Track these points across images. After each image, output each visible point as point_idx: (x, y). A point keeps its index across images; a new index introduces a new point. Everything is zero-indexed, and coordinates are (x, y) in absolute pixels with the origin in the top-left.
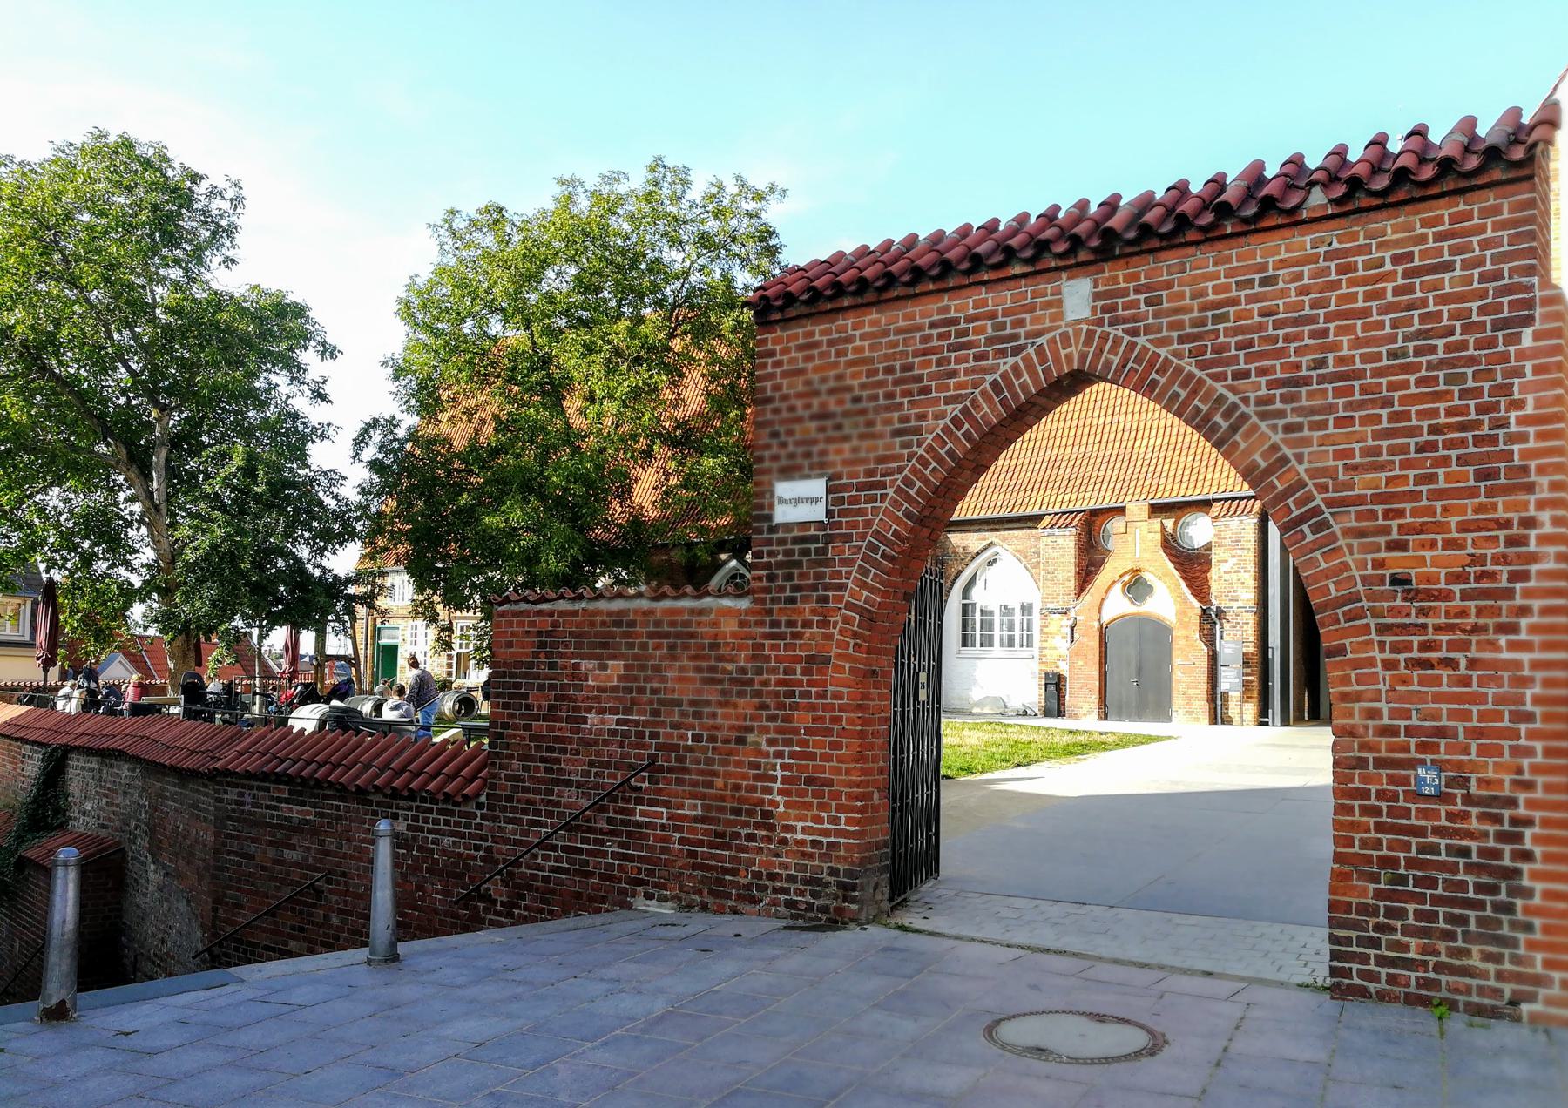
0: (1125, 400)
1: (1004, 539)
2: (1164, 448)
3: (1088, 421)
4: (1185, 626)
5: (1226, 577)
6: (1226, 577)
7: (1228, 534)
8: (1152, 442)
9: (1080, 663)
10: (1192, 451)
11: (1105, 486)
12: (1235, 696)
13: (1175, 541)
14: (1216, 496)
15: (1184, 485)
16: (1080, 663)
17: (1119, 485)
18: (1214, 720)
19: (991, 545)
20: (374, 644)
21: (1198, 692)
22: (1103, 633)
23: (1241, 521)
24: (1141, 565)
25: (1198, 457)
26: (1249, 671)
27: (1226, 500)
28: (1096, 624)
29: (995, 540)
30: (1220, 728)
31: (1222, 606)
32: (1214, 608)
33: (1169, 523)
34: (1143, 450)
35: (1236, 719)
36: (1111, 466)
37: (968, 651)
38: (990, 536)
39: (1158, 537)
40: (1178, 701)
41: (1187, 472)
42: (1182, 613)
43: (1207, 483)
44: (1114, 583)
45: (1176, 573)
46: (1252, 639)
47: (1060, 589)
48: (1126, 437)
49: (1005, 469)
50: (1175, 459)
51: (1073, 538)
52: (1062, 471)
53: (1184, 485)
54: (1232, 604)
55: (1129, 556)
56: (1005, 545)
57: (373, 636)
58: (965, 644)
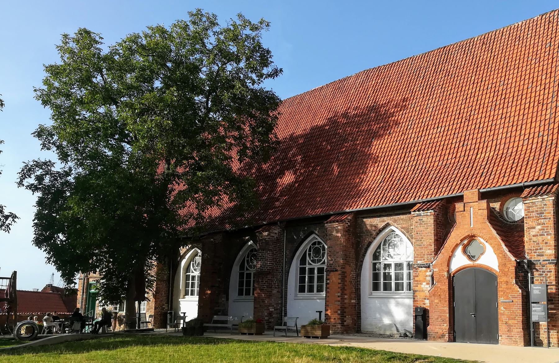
0: (472, 132)
1: (395, 221)
2: (495, 157)
3: (449, 146)
4: (505, 274)
5: (535, 239)
6: (535, 239)
7: (535, 209)
8: (487, 155)
9: (436, 301)
10: (512, 158)
11: (455, 183)
12: (543, 324)
13: (502, 216)
14: (526, 184)
15: (506, 179)
16: (436, 301)
17: (464, 182)
18: (527, 343)
19: (388, 225)
20: (87, 292)
21: (516, 322)
22: (451, 279)
23: (543, 199)
24: (475, 232)
25: (516, 161)
26: (552, 306)
27: (533, 186)
28: (446, 274)
29: (390, 222)
30: (532, 349)
31: (533, 260)
32: (526, 261)
33: (496, 205)
34: (481, 160)
35: (545, 342)
36: (460, 171)
37: (376, 293)
38: (387, 220)
39: (485, 212)
40: (502, 328)
41: (508, 170)
42: (502, 265)
43: (521, 176)
44: (457, 246)
45: (498, 237)
46: (554, 283)
47: (426, 252)
48: (471, 153)
49: (398, 178)
50: (501, 163)
51: (432, 217)
52: (430, 177)
53: (506, 179)
54: (539, 258)
55: (466, 226)
56: (395, 225)
57: (87, 288)
58: (302, 290)
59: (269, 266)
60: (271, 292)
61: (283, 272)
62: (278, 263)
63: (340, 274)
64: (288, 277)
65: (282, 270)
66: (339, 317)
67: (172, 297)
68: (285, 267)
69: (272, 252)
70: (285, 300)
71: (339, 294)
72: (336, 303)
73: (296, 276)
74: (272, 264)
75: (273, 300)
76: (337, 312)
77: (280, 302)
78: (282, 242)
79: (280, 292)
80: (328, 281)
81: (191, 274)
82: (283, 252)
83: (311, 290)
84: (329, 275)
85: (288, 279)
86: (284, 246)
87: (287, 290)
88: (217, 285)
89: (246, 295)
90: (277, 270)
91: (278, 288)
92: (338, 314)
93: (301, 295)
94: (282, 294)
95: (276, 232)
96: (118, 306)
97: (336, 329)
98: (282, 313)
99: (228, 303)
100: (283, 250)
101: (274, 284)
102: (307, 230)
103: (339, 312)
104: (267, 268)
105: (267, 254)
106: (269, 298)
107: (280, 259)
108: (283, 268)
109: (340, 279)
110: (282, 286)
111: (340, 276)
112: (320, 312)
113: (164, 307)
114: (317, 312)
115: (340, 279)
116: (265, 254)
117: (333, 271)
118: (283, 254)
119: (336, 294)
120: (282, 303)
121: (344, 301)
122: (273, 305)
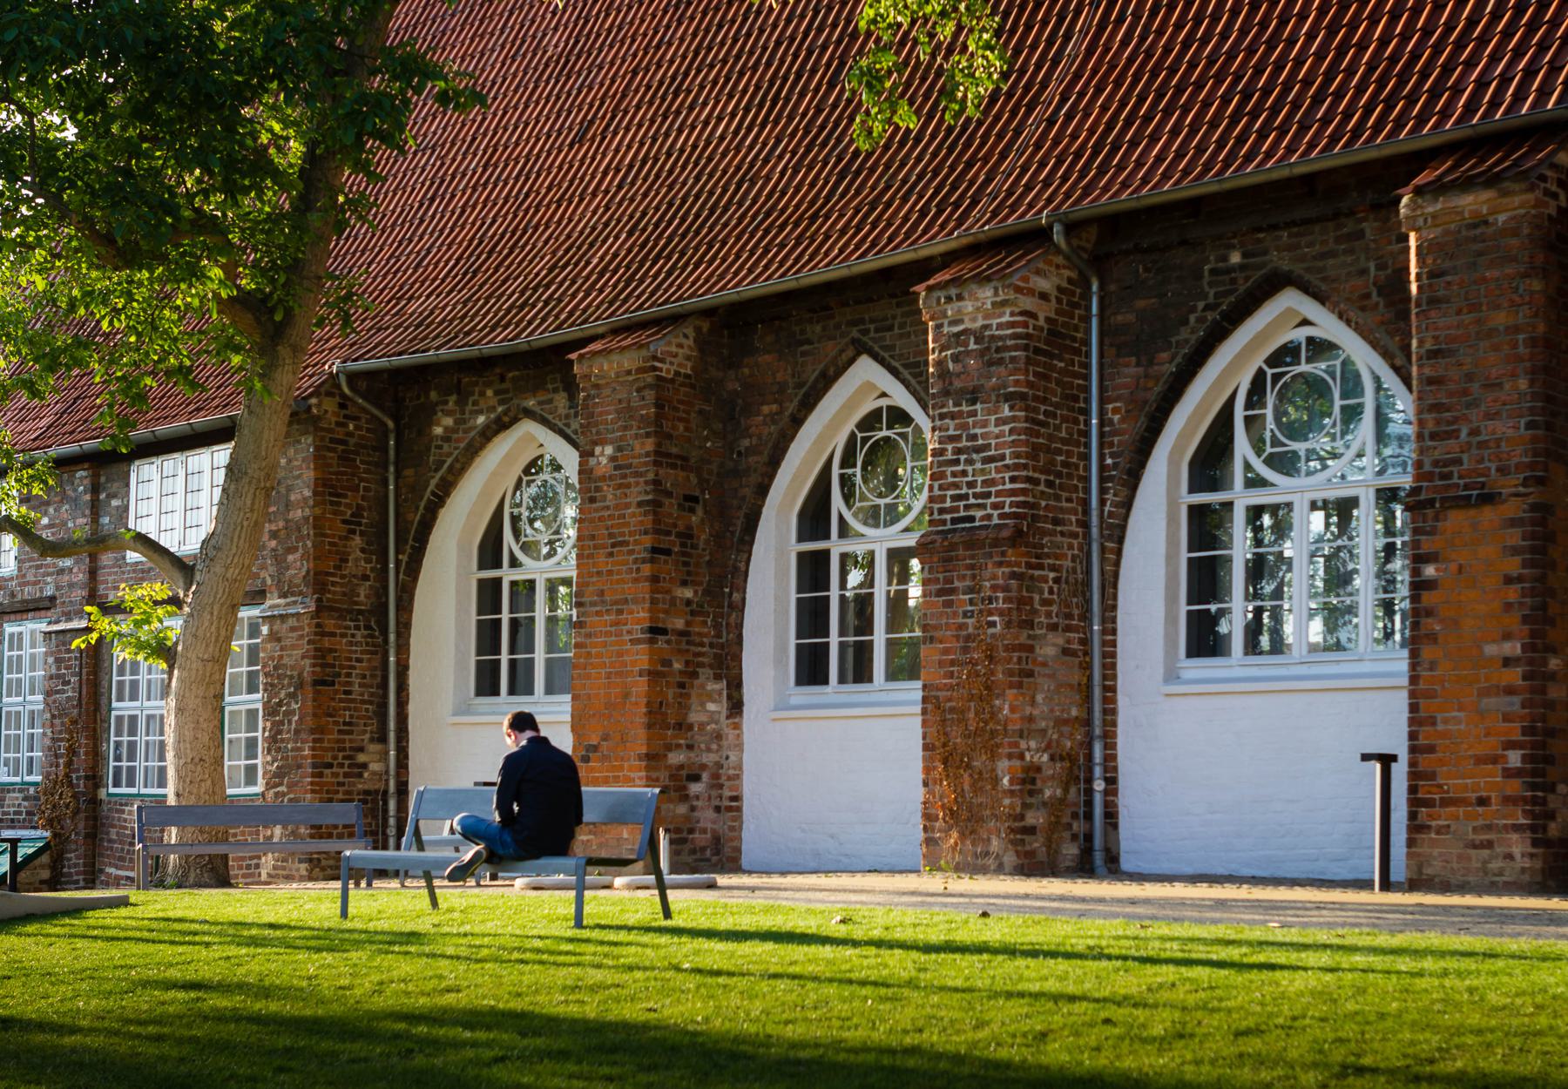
59: (1013, 493)
60: (1031, 649)
61: (1087, 535)
62: (1059, 475)
63: (1513, 522)
64: (1117, 564)
65: (1085, 525)
66: (1515, 787)
67: (402, 703)
68: (1102, 502)
69: (1027, 409)
70: (1105, 700)
71: (1513, 648)
72: (1491, 702)
73: (1171, 557)
74: (1028, 480)
75: (1039, 698)
76: (1495, 760)
77: (1074, 712)
78: (1077, 352)
79: (1073, 653)
80: (1430, 571)
81: (507, 575)
82: (1086, 412)
83: (859, 669)
84: (1432, 532)
85: (1116, 575)
86: (1087, 377)
87: (1114, 644)
88: (679, 624)
89: (842, 680)
90: (1056, 522)
91: (1068, 629)
92: (1509, 773)
93: (812, 693)
94: (1087, 667)
95: (1043, 284)
96: (573, 356)
97: (1495, 865)
98: (1089, 780)
99: (737, 726)
100: (1087, 401)
101: (1045, 602)
102: (1242, 267)
103: (1515, 758)
104: (995, 506)
105: (999, 422)
106: (1020, 685)
107: (1069, 454)
108: (1087, 512)
109: (1515, 551)
110: (1086, 616)
111: (1515, 537)
112: (1387, 760)
113: (361, 758)
114: (1366, 757)
115: (1515, 551)
116: (985, 424)
117: (1464, 503)
118: (1087, 423)
119: (1491, 650)
120: (1088, 722)
121: (1543, 691)
122: (1044, 731)
